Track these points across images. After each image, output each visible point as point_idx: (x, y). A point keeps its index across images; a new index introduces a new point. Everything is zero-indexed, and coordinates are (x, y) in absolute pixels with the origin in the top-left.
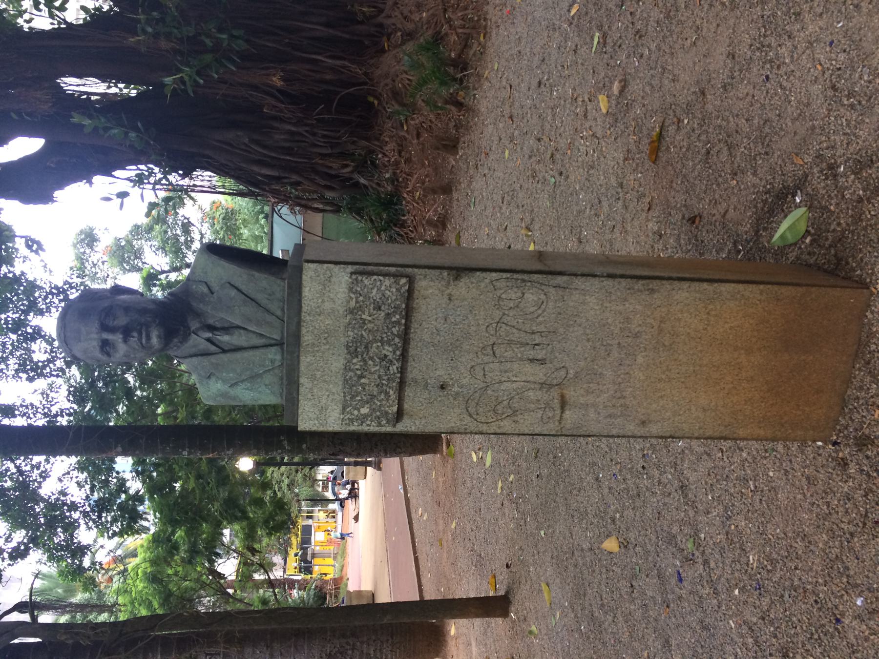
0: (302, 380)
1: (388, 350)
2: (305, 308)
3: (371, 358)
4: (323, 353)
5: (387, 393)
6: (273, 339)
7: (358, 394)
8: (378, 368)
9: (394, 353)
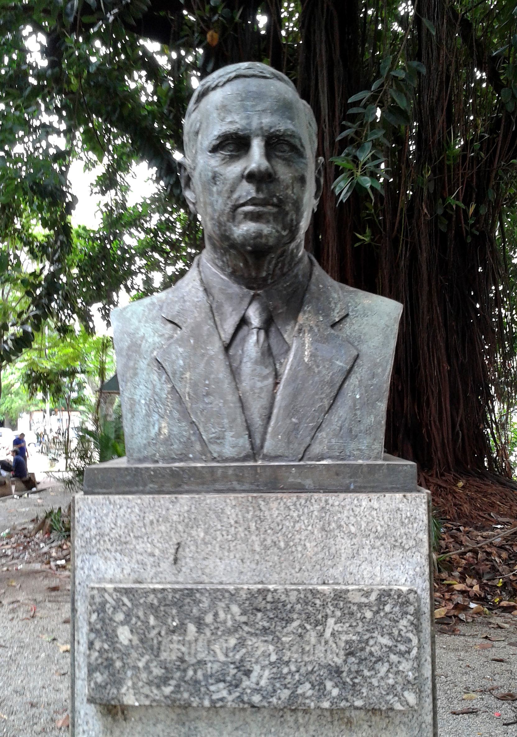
0: (184, 498)
1: (261, 676)
2: (335, 499)
3: (242, 643)
4: (245, 540)
5: (165, 680)
6: (263, 440)
7: (162, 619)
8: (222, 658)
9: (258, 691)
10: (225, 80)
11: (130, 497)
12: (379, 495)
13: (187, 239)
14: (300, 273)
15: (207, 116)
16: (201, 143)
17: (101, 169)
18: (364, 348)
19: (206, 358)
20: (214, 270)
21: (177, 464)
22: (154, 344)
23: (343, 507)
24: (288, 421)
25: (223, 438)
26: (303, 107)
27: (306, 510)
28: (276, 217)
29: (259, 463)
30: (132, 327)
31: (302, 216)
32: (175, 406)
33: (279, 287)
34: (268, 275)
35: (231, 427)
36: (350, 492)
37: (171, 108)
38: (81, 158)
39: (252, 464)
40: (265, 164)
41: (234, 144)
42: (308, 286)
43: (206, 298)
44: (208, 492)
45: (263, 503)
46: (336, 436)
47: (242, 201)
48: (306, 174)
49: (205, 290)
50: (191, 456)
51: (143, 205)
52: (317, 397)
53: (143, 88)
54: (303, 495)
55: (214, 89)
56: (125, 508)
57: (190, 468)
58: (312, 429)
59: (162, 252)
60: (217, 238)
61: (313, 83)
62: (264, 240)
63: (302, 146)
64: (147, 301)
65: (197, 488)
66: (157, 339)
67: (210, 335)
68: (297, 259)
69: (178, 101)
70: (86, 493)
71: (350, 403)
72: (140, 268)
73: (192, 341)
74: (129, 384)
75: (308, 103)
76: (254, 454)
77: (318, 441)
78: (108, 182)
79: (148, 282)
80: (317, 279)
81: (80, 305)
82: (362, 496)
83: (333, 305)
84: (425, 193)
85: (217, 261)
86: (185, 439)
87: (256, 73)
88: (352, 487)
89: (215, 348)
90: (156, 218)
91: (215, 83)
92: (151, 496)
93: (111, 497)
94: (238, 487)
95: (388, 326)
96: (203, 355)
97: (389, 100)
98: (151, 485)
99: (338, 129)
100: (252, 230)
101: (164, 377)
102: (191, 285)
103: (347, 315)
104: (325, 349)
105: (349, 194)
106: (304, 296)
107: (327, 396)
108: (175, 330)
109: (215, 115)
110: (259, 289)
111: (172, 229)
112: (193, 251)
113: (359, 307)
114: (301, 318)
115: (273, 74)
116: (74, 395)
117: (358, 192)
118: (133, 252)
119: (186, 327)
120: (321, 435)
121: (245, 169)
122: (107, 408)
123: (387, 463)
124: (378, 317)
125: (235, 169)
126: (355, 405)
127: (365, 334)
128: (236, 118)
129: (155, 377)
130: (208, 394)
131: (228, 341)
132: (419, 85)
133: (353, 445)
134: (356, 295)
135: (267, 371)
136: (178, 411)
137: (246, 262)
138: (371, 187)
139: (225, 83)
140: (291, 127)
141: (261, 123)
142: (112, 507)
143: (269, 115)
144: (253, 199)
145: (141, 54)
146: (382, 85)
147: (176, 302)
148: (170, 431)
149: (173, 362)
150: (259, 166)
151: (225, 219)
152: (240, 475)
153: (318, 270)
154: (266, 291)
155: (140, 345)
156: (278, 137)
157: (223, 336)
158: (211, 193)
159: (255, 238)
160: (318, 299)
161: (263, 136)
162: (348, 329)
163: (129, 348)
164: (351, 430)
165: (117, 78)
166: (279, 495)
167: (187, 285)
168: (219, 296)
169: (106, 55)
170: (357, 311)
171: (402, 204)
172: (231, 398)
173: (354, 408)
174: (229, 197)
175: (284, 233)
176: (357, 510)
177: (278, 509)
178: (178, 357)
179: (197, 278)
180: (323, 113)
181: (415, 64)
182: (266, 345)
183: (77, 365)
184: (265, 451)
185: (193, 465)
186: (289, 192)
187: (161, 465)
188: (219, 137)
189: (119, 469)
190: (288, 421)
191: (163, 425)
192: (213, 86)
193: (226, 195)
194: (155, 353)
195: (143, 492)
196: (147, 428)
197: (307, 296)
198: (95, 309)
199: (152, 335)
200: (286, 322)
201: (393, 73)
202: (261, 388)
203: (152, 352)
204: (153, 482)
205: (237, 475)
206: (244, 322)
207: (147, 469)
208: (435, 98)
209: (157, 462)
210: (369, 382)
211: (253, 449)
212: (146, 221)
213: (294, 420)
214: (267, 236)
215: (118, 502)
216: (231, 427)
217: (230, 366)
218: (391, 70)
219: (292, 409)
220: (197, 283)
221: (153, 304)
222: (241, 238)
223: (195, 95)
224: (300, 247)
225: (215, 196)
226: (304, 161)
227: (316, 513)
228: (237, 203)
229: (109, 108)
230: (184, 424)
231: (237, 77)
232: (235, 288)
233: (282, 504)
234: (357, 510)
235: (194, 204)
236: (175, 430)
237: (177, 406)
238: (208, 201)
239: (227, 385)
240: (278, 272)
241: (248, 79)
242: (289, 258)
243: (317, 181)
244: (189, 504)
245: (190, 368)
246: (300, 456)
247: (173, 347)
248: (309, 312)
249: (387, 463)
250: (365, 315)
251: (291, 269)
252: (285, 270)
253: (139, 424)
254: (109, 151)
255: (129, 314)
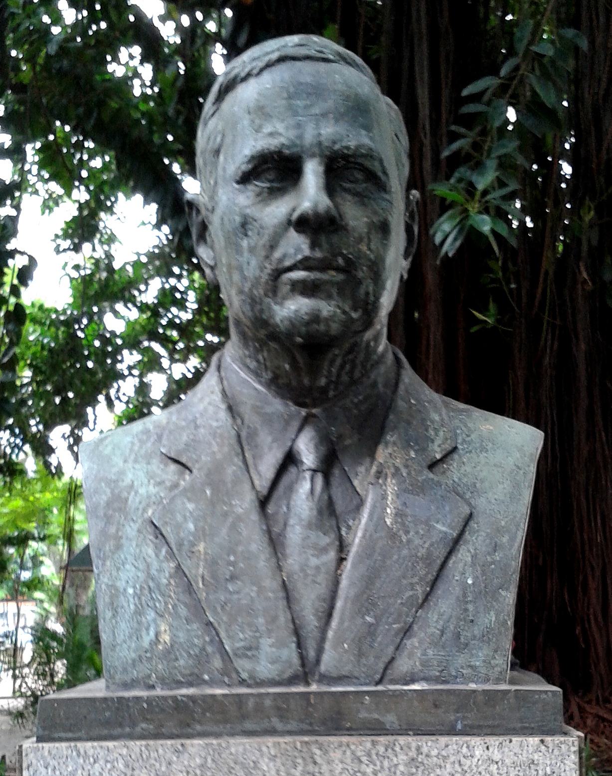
0: (196, 745)
2: (431, 746)
6: (320, 650)
10: (261, 64)
11: (111, 744)
12: (501, 739)
13: (205, 320)
14: (380, 381)
15: (233, 123)
16: (224, 169)
17: (68, 210)
18: (481, 503)
19: (230, 520)
20: (242, 374)
21: (184, 691)
22: (149, 497)
23: (445, 758)
24: (359, 621)
25: (257, 648)
26: (387, 109)
27: (386, 764)
28: (341, 288)
29: (314, 688)
30: (115, 470)
31: (383, 288)
32: (182, 597)
33: (347, 402)
34: (328, 384)
35: (269, 631)
36: (456, 735)
37: (179, 107)
38: (36, 192)
39: (301, 689)
40: (325, 202)
41: (276, 170)
42: (392, 400)
43: (230, 420)
44: (232, 735)
45: (318, 752)
46: (434, 644)
47: (288, 263)
48: (390, 219)
49: (230, 409)
50: (206, 677)
51: (137, 264)
52: (405, 582)
53: (136, 75)
54: (382, 739)
55: (245, 79)
56: (102, 762)
57: (205, 697)
58: (396, 634)
59: (165, 341)
60: (249, 324)
61: (406, 64)
62: (322, 327)
63: (385, 173)
64: (138, 426)
65: (215, 729)
66: (152, 489)
67: (236, 482)
68: (375, 357)
69: (189, 93)
70: (40, 739)
71: (458, 591)
72: (130, 368)
73: (208, 492)
74: (108, 563)
75: (396, 102)
76: (306, 674)
77: (406, 653)
78: (83, 229)
79: (143, 389)
80: (407, 391)
81: (34, 429)
82: (475, 741)
83: (432, 432)
84: (585, 248)
85: (248, 361)
86: (197, 651)
87: (312, 53)
88: (459, 726)
89: (244, 503)
90: (156, 284)
91: (247, 70)
92: (144, 743)
93: (79, 745)
94: (279, 726)
95: (518, 467)
96: (225, 515)
97: (528, 94)
98: (144, 725)
99: (444, 139)
100: (304, 310)
101: (164, 551)
102: (207, 400)
103: (455, 449)
104: (420, 504)
105: (458, 243)
106: (386, 417)
107: (421, 579)
108: (181, 474)
109: (246, 122)
110: (314, 406)
111: (181, 304)
112: (216, 340)
113: (473, 436)
114: (382, 454)
115: (339, 54)
116: (26, 575)
117: (472, 239)
118: (119, 341)
119: (199, 469)
120: (412, 643)
121: (294, 210)
122: (77, 595)
123: (514, 688)
124: (504, 452)
125: (277, 211)
126: (465, 595)
127: (482, 481)
128: (280, 127)
129: (150, 551)
130: (233, 578)
131: (265, 492)
132: (576, 70)
133: (461, 660)
134: (469, 416)
135: (325, 540)
136: (186, 605)
137: (294, 363)
138: (493, 231)
139: (262, 70)
140: (366, 141)
141: (320, 134)
142: (81, 761)
143: (332, 122)
144: (306, 259)
145: (132, 18)
146: (517, 68)
147: (183, 428)
148: (174, 637)
149: (178, 527)
150: (316, 205)
151: (262, 292)
152: (282, 707)
153: (409, 376)
154: (325, 410)
155: (127, 500)
156: (345, 157)
157: (257, 482)
158: (238, 250)
159: (308, 324)
160: (409, 423)
161: (322, 156)
162: (456, 471)
163: (108, 504)
164: (458, 636)
165: (94, 60)
166: (345, 739)
167: (201, 399)
168: (251, 418)
169: (77, 24)
170: (469, 443)
171: (547, 264)
172: (271, 584)
173: (463, 600)
174: (267, 257)
175: (355, 315)
176: (467, 763)
177: (342, 762)
178: (187, 517)
179: (217, 390)
180: (421, 115)
181: (570, 33)
182: (326, 497)
183: (32, 527)
184: (323, 668)
185: (209, 691)
186: (364, 248)
187: (159, 692)
188: (253, 158)
189: (93, 700)
190: (359, 621)
191: (163, 629)
192: (243, 75)
193: (263, 253)
194: (150, 512)
195: (132, 737)
196: (138, 631)
197: (391, 417)
198: (58, 436)
199: (145, 482)
200: (357, 459)
201: (534, 48)
202: (317, 568)
203: (145, 510)
204: (146, 720)
205: (279, 709)
206: (290, 459)
207: (138, 699)
208: (602, 92)
209: (153, 687)
210: (489, 559)
211: (303, 665)
212: (140, 292)
213: (368, 619)
214: (327, 320)
215: (91, 752)
216: (269, 631)
217: (269, 532)
218: (531, 43)
219: (365, 601)
220: (217, 397)
221: (147, 432)
222: (286, 323)
223: (215, 89)
224: (380, 340)
225: (246, 254)
226: (387, 196)
227: (401, 768)
228: (280, 266)
229: (81, 110)
230: (195, 626)
231: (282, 59)
232: (277, 405)
233: (348, 753)
234: (467, 763)
235: (212, 268)
236: (182, 636)
237: (185, 598)
238: (234, 263)
239: (263, 562)
240: (345, 378)
241: (298, 64)
242: (361, 356)
243: (409, 229)
244: (203, 754)
245: (204, 535)
246: (378, 677)
247: (178, 502)
248: (394, 443)
249: (514, 688)
250: (483, 449)
251: (365, 374)
252: (357, 374)
253: (124, 628)
254: (81, 180)
255: (109, 448)
